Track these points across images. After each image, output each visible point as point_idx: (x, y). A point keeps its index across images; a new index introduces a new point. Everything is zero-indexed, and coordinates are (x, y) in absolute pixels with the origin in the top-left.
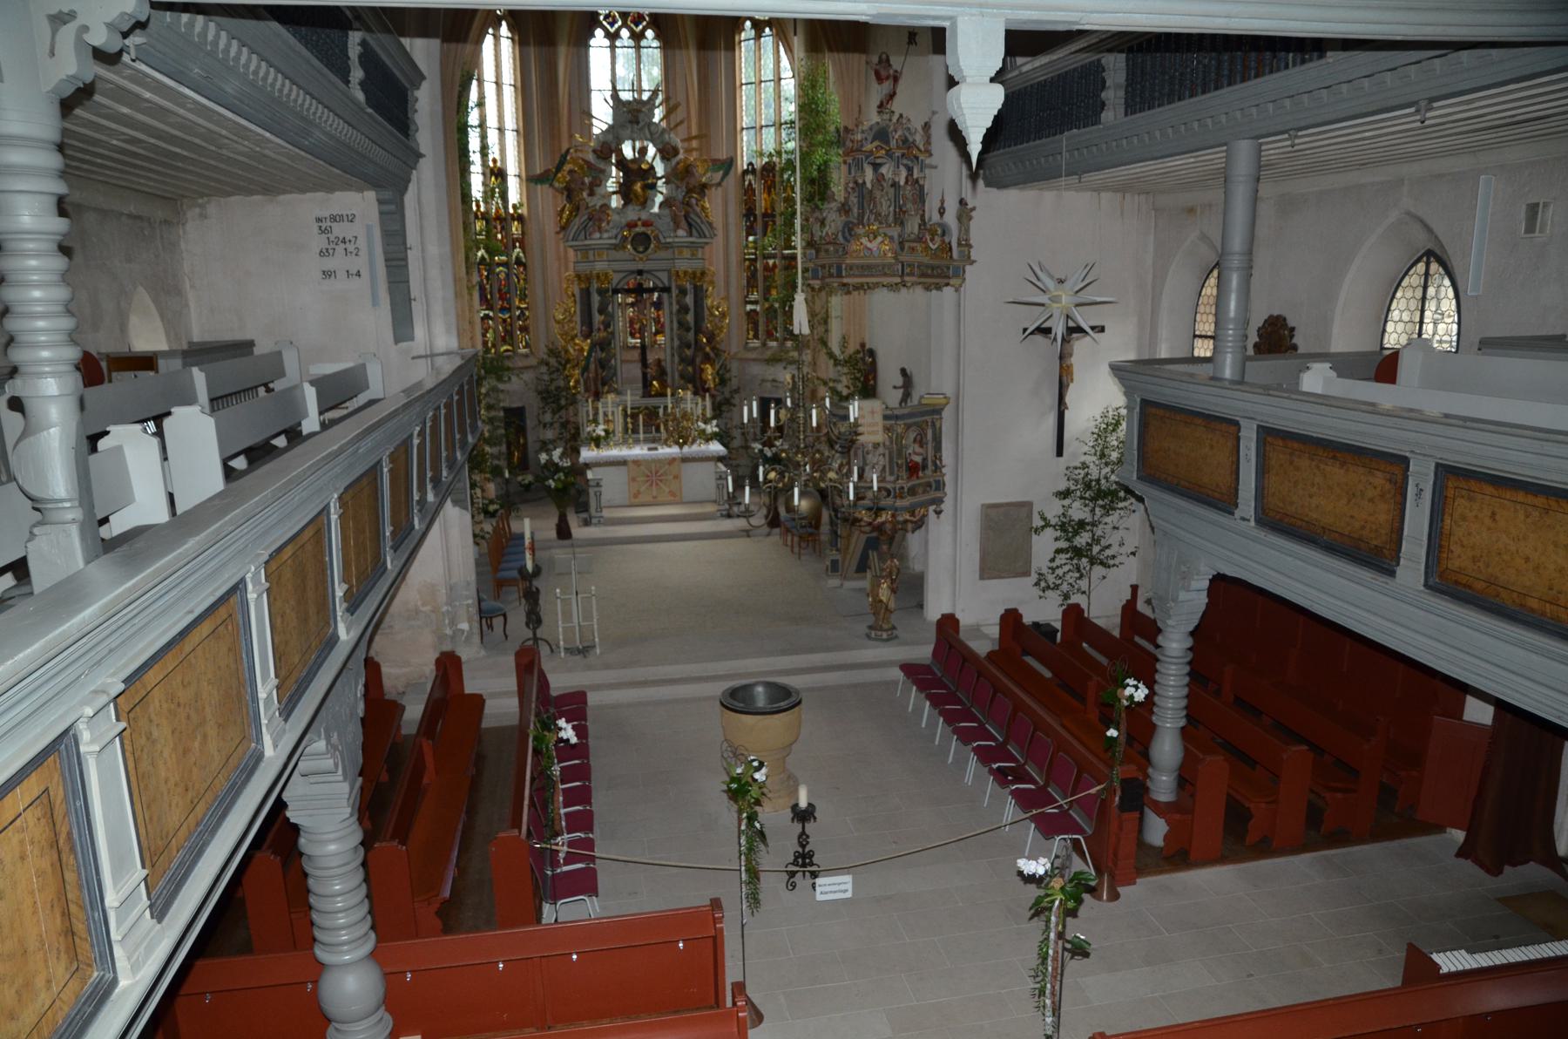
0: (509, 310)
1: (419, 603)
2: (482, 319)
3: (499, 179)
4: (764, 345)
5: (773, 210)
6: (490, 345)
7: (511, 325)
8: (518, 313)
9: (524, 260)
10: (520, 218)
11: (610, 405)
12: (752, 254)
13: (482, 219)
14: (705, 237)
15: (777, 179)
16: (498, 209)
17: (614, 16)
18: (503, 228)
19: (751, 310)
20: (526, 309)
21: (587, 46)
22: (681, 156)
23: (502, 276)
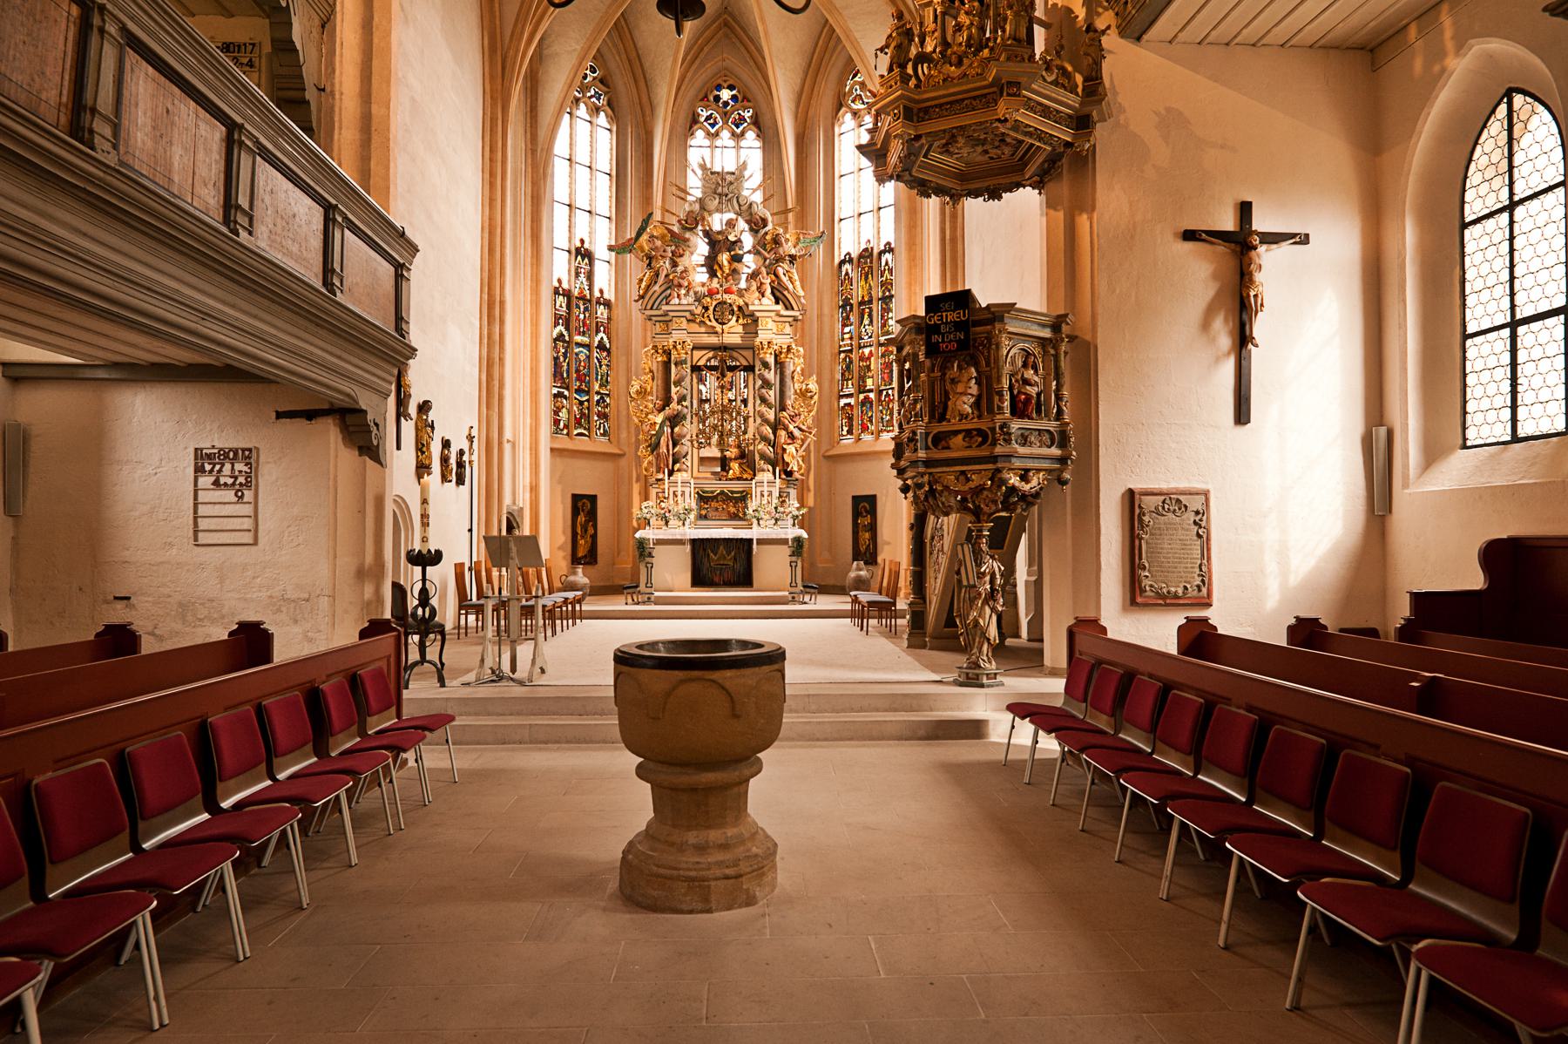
0: (588, 393)
2: (555, 396)
3: (586, 260)
5: (871, 297)
7: (588, 408)
8: (597, 398)
9: (608, 346)
10: (607, 304)
11: (679, 484)
13: (564, 295)
14: (793, 309)
15: (875, 264)
18: (586, 309)
19: (846, 404)
20: (608, 395)
22: (770, 227)
23: (582, 357)
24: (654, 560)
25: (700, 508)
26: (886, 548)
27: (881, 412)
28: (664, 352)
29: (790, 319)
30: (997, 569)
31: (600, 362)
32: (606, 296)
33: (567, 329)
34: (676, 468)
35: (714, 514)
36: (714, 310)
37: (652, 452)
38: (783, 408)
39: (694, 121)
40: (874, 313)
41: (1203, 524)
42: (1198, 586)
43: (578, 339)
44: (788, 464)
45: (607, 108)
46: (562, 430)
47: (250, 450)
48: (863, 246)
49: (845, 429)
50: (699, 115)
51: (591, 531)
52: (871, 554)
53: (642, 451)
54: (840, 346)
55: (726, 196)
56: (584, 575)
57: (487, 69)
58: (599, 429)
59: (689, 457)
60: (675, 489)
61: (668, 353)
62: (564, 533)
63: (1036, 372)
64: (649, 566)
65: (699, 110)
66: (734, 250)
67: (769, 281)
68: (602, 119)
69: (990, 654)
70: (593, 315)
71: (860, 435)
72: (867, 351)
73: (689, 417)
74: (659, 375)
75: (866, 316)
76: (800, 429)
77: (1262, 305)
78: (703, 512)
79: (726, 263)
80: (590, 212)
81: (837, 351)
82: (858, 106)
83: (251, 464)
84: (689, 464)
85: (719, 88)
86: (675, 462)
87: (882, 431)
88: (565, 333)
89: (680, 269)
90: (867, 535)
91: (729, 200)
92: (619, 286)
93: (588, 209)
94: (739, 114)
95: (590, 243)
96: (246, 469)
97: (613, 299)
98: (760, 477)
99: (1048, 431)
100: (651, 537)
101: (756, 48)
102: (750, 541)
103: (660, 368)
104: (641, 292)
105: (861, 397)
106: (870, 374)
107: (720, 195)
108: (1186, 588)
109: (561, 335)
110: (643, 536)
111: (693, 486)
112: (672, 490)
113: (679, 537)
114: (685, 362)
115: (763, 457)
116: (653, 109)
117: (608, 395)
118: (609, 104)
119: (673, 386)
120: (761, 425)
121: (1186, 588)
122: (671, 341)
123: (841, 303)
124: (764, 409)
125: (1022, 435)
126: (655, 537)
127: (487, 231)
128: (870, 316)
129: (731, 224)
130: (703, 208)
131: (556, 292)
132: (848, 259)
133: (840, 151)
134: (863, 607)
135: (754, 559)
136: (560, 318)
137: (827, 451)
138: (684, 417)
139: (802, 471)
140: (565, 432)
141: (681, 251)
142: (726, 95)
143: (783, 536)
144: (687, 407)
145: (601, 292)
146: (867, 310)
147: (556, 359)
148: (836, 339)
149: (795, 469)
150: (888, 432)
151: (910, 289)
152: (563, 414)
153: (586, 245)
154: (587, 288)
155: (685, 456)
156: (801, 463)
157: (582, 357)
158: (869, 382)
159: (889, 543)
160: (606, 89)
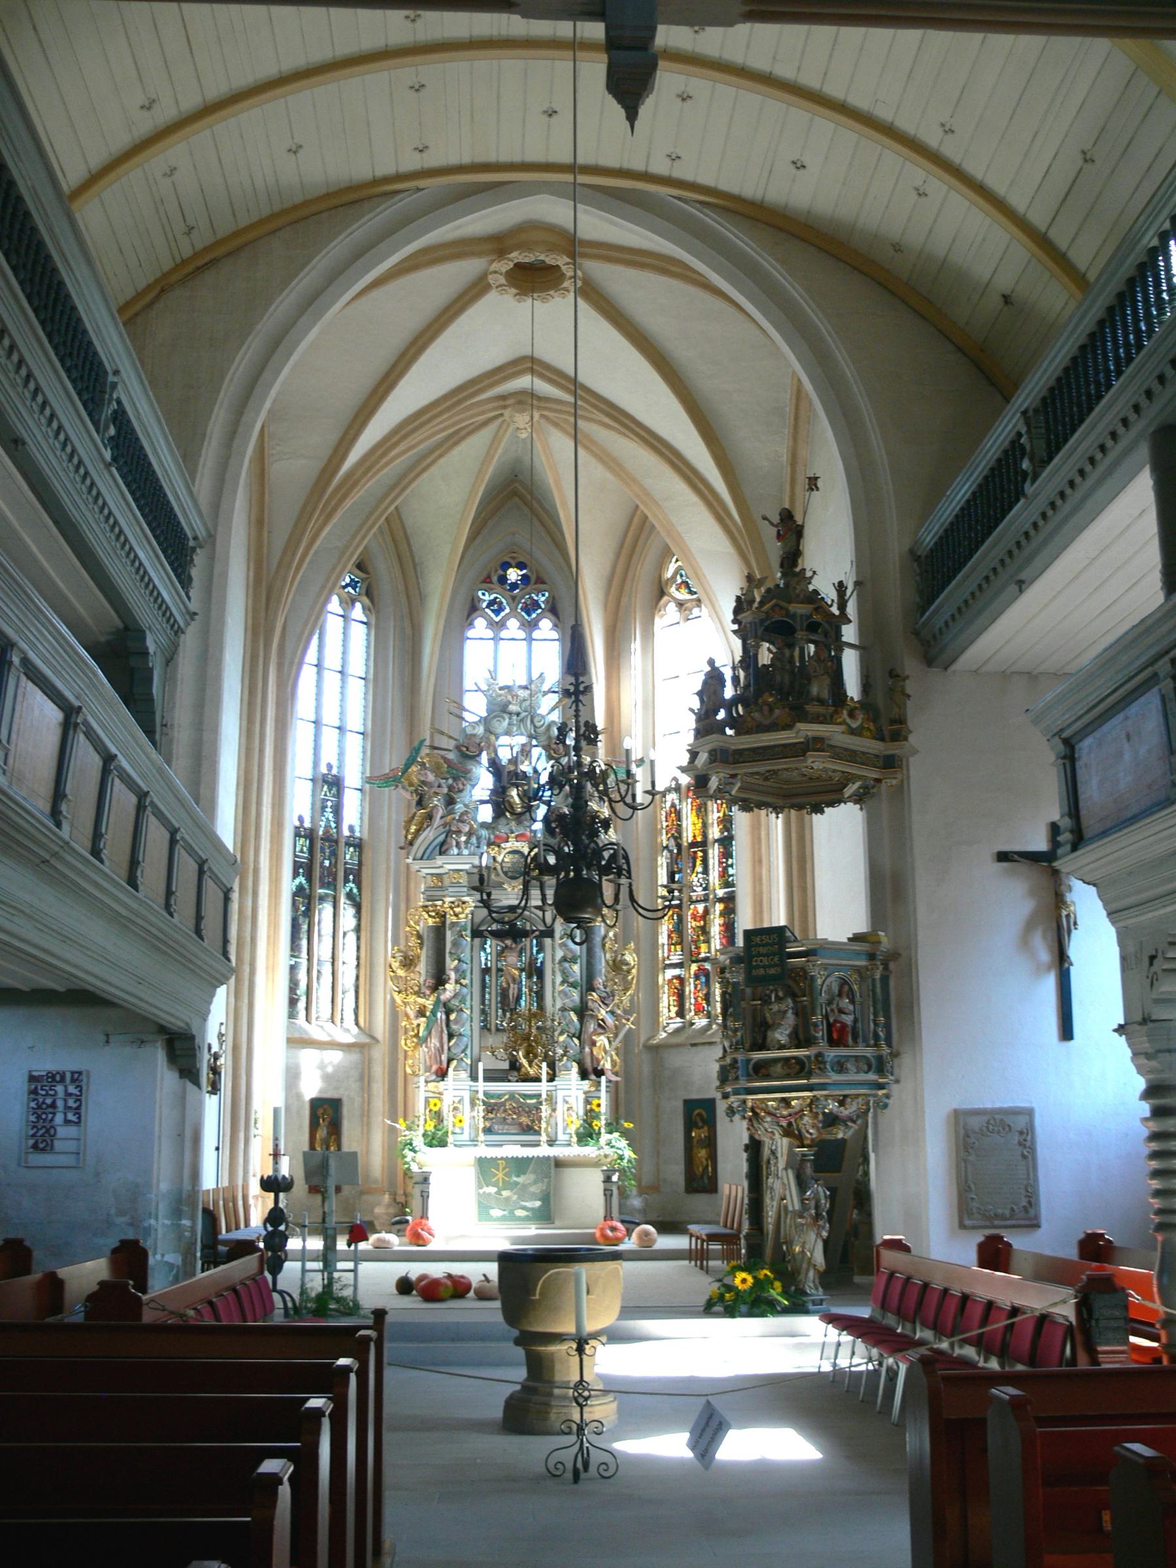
1: (113, 1211)
13: (305, 837)
16: (328, 827)
17: (501, 603)
21: (463, 639)
30: (822, 1194)
38: (591, 988)
39: (473, 608)
41: (1028, 1144)
42: (1025, 1207)
47: (80, 1073)
50: (480, 600)
52: (709, 1178)
57: (250, 602)
63: (852, 1002)
65: (480, 593)
68: (358, 612)
69: (817, 1281)
75: (698, 862)
77: (1075, 923)
80: (339, 728)
83: (81, 1087)
85: (506, 566)
89: (459, 807)
91: (522, 720)
94: (531, 598)
95: (339, 767)
96: (76, 1092)
97: (365, 836)
99: (864, 1057)
101: (554, 522)
104: (410, 837)
108: (1012, 1210)
116: (422, 598)
121: (1012, 1210)
125: (838, 1062)
127: (242, 787)
129: (525, 751)
130: (488, 731)
131: (297, 835)
134: (703, 1241)
136: (301, 867)
137: (649, 1039)
139: (617, 1068)
141: (461, 786)
142: (513, 575)
144: (465, 986)
145: (351, 828)
146: (700, 854)
154: (333, 825)
156: (615, 1057)
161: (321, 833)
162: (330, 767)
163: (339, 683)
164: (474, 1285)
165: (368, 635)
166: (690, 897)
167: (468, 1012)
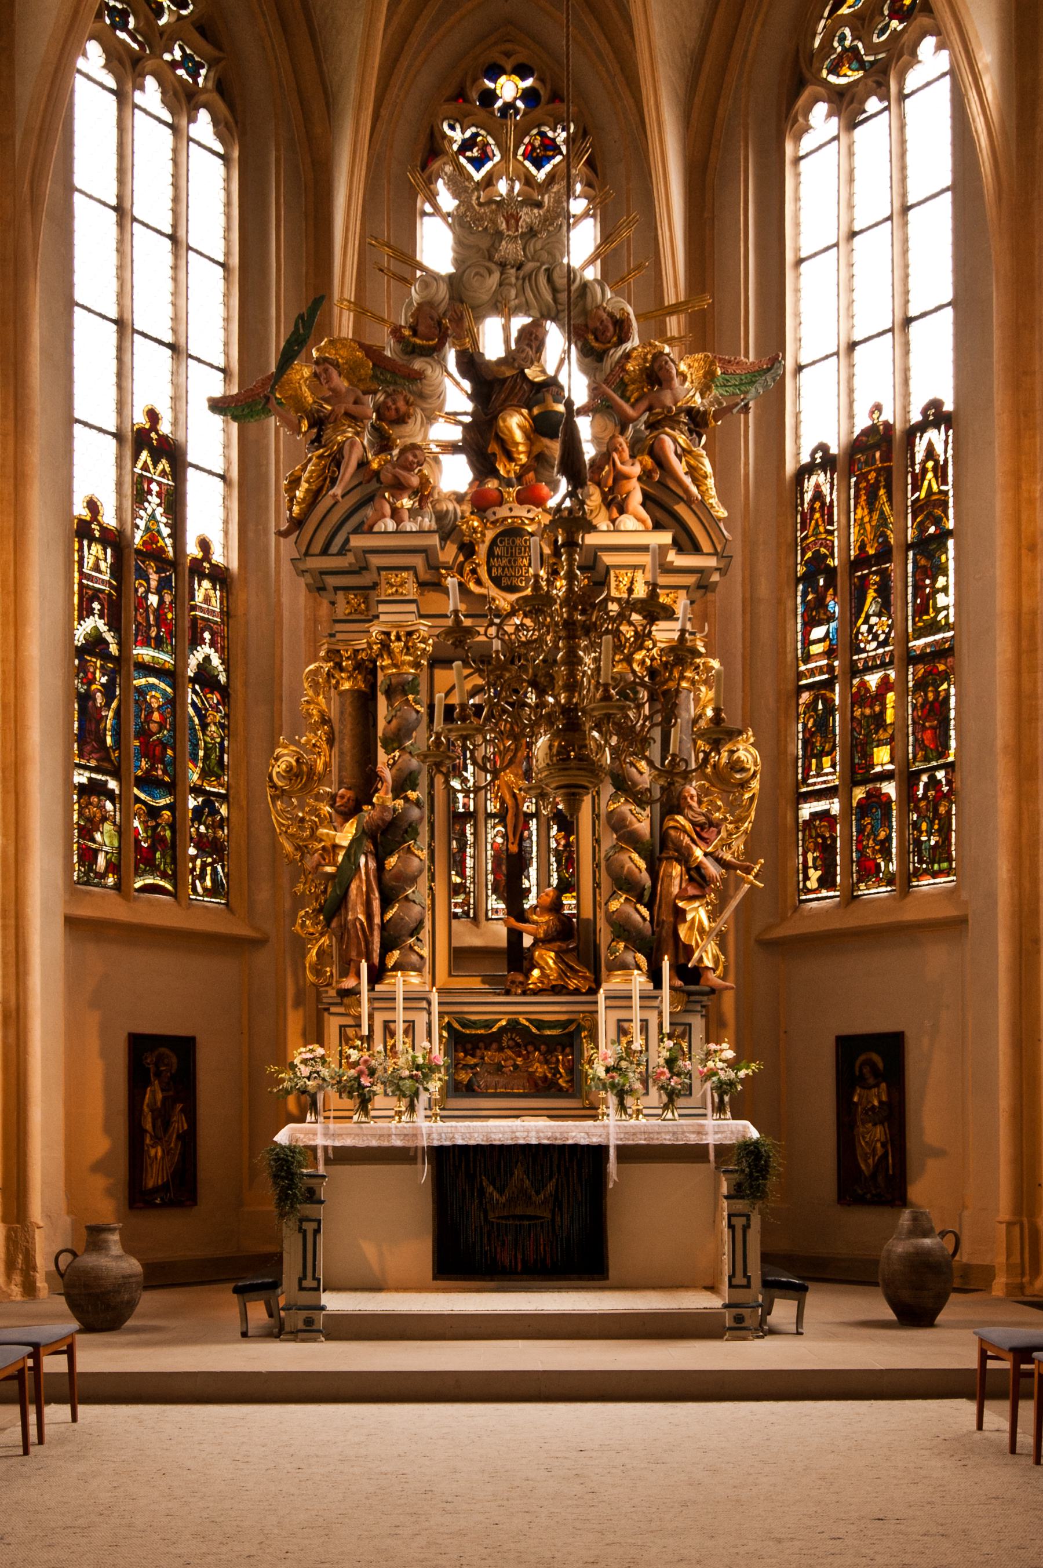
0: (170, 788)
3: (164, 464)
4: (851, 898)
6: (101, 861)
8: (192, 803)
9: (222, 678)
10: (220, 577)
11: (400, 1003)
12: (820, 670)
14: (697, 549)
16: (152, 535)
19: (814, 815)
20: (224, 798)
23: (155, 699)
24: (322, 1211)
25: (455, 1066)
26: (933, 1165)
27: (916, 826)
28: (359, 666)
29: (690, 580)
31: (202, 718)
32: (218, 557)
33: (114, 625)
34: (390, 963)
35: (492, 1079)
36: (490, 553)
37: (328, 924)
40: (896, 583)
43: (145, 653)
44: (689, 950)
45: (215, 98)
46: (103, 876)
48: (862, 422)
49: (814, 875)
51: (179, 1123)
53: (306, 922)
54: (800, 675)
55: (519, 267)
56: (129, 1249)
58: (202, 877)
59: (425, 934)
60: (387, 1016)
61: (367, 669)
62: (108, 1129)
64: (310, 1227)
66: (542, 401)
67: (636, 470)
68: (203, 127)
70: (184, 598)
71: (854, 887)
72: (873, 680)
73: (424, 829)
74: (346, 729)
75: (871, 594)
76: (720, 861)
78: (464, 1077)
79: (519, 436)
80: (173, 347)
81: (791, 687)
82: (849, 76)
84: (425, 952)
85: (495, 72)
86: (387, 947)
87: (917, 874)
88: (109, 637)
90: (879, 1132)
91: (529, 276)
92: (251, 535)
93: (168, 338)
94: (542, 134)
95: (175, 423)
97: (234, 565)
98: (613, 983)
100: (320, 1141)
102: (600, 1151)
103: (349, 709)
105: (859, 793)
106: (883, 735)
107: (503, 265)
109: (95, 643)
110: (304, 1140)
111: (435, 1009)
112: (379, 1018)
113: (398, 1143)
114: (412, 686)
115: (622, 929)
117: (224, 798)
118: (221, 87)
119: (381, 751)
120: (618, 849)
122: (375, 630)
123: (801, 570)
124: (625, 808)
126: (329, 1143)
128: (884, 591)
132: (826, 461)
133: (797, 199)
135: (610, 1201)
137: (769, 928)
138: (411, 831)
140: (111, 880)
143: (693, 1139)
144: (418, 803)
145: (204, 545)
147: (84, 699)
148: (790, 657)
149: (708, 962)
150: (935, 875)
151: (1018, 488)
152: (105, 837)
153: (165, 428)
154: (166, 531)
155: (415, 931)
157: (155, 699)
158: (882, 756)
159: (938, 1153)
160: (216, 53)
161: (137, 540)
162: (153, 416)
163: (169, 259)
164: (613, 1143)
165: (228, 180)
166: (854, 663)
167: (424, 854)
